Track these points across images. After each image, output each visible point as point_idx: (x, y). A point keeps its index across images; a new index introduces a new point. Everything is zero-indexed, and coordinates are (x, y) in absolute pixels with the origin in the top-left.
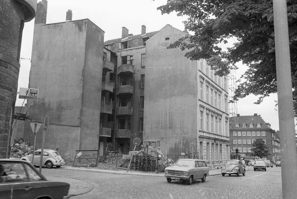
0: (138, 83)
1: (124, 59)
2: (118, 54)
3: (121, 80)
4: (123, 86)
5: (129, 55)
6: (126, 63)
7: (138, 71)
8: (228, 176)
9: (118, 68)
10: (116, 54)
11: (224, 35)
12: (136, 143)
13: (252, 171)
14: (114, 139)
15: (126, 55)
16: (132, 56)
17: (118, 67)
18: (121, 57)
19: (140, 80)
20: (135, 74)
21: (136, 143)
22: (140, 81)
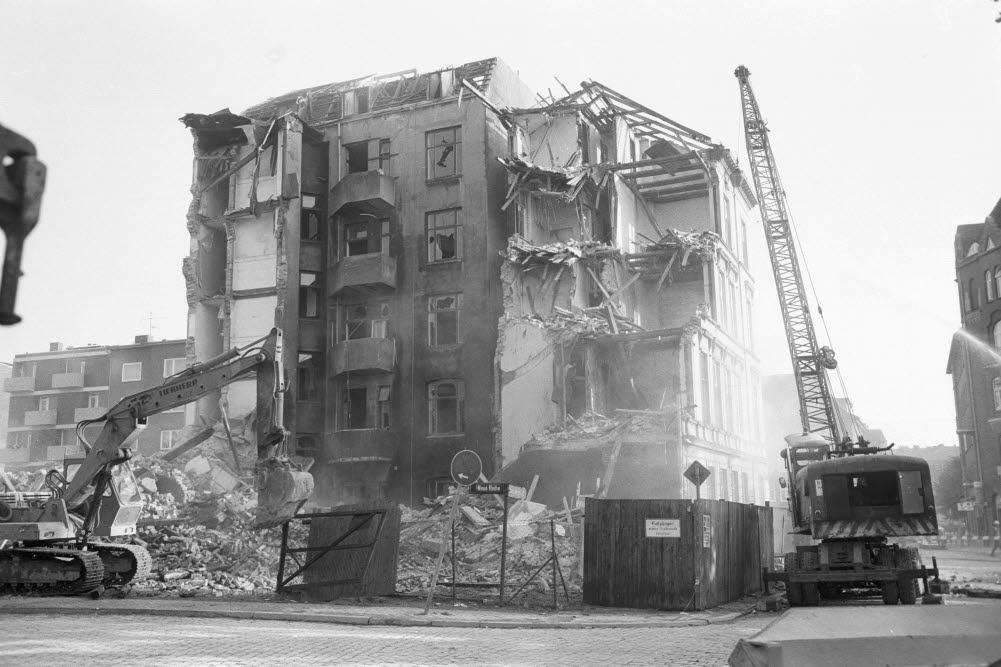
0: (414, 246)
1: (358, 157)
2: (331, 135)
3: (345, 237)
4: (355, 258)
5: (375, 139)
6: (366, 169)
7: (414, 198)
8: (363, 78)
9: (332, 191)
10: (321, 136)
11: (654, 529)
12: (461, 476)
13: (839, 373)
14: (29, 550)
15: (362, 139)
16: (386, 141)
17: (332, 183)
18: (343, 146)
19: (423, 233)
20: (400, 210)
21: (461, 476)
22: (420, 236)
